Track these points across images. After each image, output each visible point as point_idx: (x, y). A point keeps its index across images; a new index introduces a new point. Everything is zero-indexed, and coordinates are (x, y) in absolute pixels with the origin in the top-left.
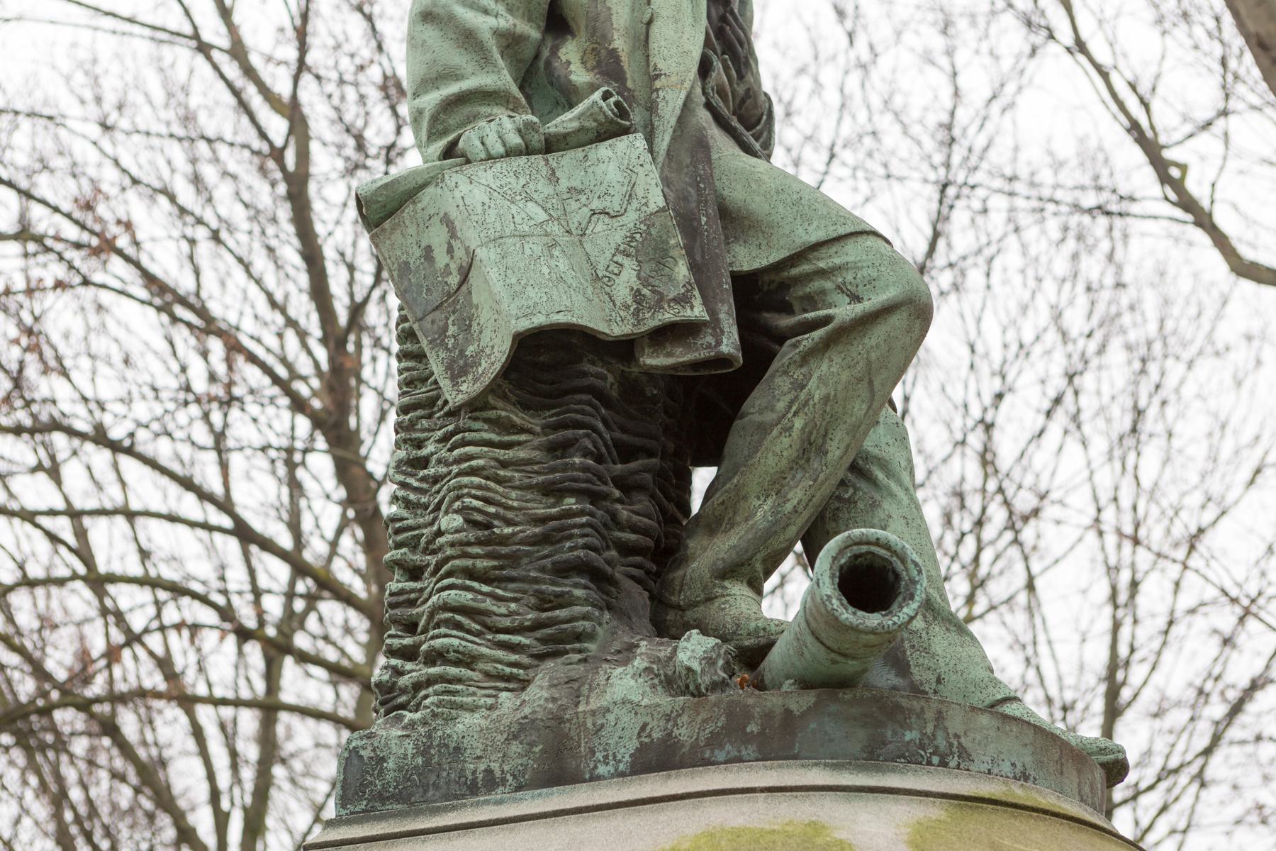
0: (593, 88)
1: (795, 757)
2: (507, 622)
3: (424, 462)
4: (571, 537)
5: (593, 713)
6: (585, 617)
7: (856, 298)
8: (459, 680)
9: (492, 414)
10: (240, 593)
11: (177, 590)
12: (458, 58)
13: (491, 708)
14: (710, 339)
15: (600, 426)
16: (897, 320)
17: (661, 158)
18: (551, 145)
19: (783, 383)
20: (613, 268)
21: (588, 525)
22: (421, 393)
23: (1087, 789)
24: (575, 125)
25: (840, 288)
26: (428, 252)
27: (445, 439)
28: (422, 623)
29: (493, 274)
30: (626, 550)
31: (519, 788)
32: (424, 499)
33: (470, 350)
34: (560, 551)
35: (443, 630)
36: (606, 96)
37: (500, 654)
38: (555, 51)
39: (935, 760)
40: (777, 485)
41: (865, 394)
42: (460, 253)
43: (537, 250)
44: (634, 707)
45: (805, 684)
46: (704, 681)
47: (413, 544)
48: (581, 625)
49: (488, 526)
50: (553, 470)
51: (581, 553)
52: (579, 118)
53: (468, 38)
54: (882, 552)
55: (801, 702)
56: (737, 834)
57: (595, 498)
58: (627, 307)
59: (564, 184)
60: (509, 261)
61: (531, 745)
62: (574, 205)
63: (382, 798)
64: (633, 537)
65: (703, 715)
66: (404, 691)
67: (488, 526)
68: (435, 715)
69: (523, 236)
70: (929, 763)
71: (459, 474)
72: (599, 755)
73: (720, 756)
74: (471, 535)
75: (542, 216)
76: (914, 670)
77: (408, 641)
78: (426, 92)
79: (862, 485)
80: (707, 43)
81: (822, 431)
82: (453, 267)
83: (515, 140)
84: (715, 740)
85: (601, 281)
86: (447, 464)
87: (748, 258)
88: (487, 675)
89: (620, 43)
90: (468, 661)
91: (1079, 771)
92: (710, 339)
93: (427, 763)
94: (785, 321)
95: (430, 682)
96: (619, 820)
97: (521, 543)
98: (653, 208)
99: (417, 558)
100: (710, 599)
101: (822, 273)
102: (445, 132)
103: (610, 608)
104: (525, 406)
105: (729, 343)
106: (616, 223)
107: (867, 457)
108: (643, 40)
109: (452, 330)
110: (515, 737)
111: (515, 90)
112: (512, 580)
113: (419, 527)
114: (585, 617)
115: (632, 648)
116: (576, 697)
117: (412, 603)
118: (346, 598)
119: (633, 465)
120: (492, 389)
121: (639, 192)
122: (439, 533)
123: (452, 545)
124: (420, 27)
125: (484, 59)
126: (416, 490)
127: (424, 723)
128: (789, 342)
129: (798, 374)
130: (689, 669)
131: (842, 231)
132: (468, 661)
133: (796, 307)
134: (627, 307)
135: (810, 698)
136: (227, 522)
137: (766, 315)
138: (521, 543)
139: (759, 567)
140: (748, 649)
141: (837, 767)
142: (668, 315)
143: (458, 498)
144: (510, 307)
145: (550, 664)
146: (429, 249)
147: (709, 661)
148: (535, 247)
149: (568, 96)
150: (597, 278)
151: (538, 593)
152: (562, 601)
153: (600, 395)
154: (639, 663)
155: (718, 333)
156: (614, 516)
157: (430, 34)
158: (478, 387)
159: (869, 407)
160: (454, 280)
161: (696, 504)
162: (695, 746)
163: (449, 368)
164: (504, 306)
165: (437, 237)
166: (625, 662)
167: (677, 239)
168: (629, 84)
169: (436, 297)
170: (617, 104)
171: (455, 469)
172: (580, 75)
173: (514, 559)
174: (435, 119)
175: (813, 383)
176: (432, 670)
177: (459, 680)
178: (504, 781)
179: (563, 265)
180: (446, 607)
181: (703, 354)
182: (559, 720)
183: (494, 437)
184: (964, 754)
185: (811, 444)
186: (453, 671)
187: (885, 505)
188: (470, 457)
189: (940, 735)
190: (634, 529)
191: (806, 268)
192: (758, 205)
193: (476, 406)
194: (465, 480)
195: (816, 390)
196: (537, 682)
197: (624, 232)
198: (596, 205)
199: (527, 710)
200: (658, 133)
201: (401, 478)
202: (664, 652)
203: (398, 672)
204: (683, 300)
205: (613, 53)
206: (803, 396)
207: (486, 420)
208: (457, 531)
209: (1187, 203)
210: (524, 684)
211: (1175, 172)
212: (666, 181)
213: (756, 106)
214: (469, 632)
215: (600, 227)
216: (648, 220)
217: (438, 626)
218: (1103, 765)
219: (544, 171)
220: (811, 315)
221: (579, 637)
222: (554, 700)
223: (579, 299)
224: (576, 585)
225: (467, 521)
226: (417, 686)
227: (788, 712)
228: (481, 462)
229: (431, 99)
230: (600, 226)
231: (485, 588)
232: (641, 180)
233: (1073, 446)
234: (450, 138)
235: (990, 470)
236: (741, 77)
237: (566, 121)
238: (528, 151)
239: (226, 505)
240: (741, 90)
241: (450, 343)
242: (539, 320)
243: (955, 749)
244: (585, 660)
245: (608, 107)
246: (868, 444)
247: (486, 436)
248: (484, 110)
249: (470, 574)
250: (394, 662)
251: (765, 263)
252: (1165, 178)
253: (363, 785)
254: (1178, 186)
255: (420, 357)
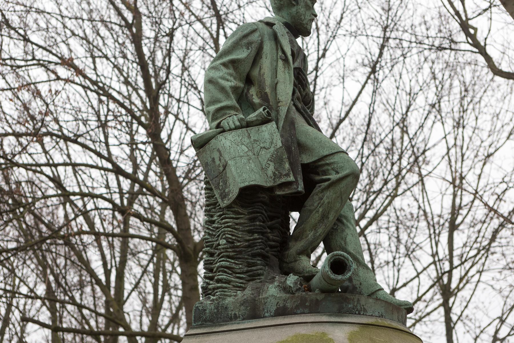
0: (261, 106)
1: (319, 313)
2: (239, 271)
3: (213, 222)
4: (256, 246)
5: (264, 298)
6: (261, 269)
7: (337, 173)
8: (226, 288)
9: (233, 209)
10: (115, 192)
11: (93, 196)
12: (220, 96)
13: (235, 296)
14: (295, 186)
15: (264, 212)
16: (349, 179)
17: (280, 129)
18: (249, 125)
19: (316, 198)
20: (267, 165)
21: (261, 242)
22: (212, 201)
23: (400, 317)
24: (255, 118)
25: (333, 169)
26: (213, 159)
27: (220, 216)
28: (215, 269)
29: (233, 169)
30: (271, 247)
31: (243, 319)
32: (214, 233)
33: (227, 190)
34: (253, 250)
35: (221, 273)
36: (264, 110)
37: (237, 280)
38: (248, 90)
39: (357, 312)
40: (315, 227)
42: (223, 161)
43: (245, 161)
44: (275, 297)
45: (323, 291)
46: (294, 289)
47: (211, 246)
48: (260, 271)
49: (233, 243)
50: (251, 226)
51: (259, 251)
52: (256, 116)
53: (222, 89)
54: (342, 258)
55: (321, 297)
56: (303, 336)
57: (262, 233)
58: (271, 177)
59: (252, 138)
60: (238, 165)
61: (247, 307)
62: (255, 145)
63: (205, 321)
64: (273, 243)
65: (294, 300)
66: (210, 289)
67: (233, 243)
68: (220, 298)
69: (241, 157)
70: (355, 314)
71: (225, 227)
72: (266, 311)
73: (299, 312)
74: (228, 246)
75: (247, 150)
76: (354, 281)
77: (210, 275)
78: (210, 106)
79: (340, 224)
80: (295, 85)
82: (221, 165)
83: (238, 123)
84: (297, 307)
85: (264, 169)
86: (221, 224)
87: (306, 159)
88: (234, 286)
89: (268, 90)
90: (228, 282)
91: (398, 312)
92: (295, 186)
93: (218, 311)
94: (318, 178)
95: (218, 288)
96: (271, 331)
97: (242, 247)
98: (278, 146)
99: (212, 251)
100: (296, 261)
101: (328, 164)
102: (216, 119)
103: (267, 265)
104: (242, 207)
105: (301, 188)
106: (268, 151)
107: (341, 216)
108: (275, 87)
109: (221, 184)
110: (242, 305)
111: (237, 105)
112: (240, 258)
113: (213, 241)
114: (261, 269)
115: (274, 278)
116: (259, 293)
117: (211, 264)
118: (153, 192)
119: (273, 222)
120: (234, 202)
121: (274, 142)
122: (219, 245)
123: (223, 249)
124: (208, 85)
125: (228, 96)
126: (211, 230)
127: (217, 300)
128: (318, 185)
129: (321, 195)
130: (290, 286)
131: (333, 151)
132: (228, 282)
133: (320, 173)
134: (271, 177)
135: (323, 296)
136: (109, 166)
137: (312, 175)
138: (242, 247)
139: (309, 251)
140: (307, 277)
141: (330, 315)
142: (283, 180)
143: (224, 234)
144: (238, 180)
145: (251, 283)
146: (214, 159)
147: (296, 283)
148: (244, 160)
149: (254, 107)
150: (262, 169)
151: (248, 263)
152: (254, 264)
153: (263, 203)
154: (276, 284)
155: (298, 185)
156: (268, 238)
157: (211, 87)
158: (229, 202)
160: (221, 169)
161: (292, 231)
162: (292, 309)
163: (221, 195)
164: (237, 179)
165: (216, 155)
166: (272, 282)
167: (285, 156)
168: (271, 103)
169: (216, 174)
170: (268, 112)
171: (223, 226)
172: (256, 100)
173: (240, 252)
174: (213, 115)
175: (325, 198)
176: (219, 285)
177: (226, 288)
178: (239, 317)
179: (253, 165)
180: (222, 267)
181: (293, 191)
182: (255, 300)
183: (234, 216)
184: (365, 310)
186: (224, 285)
187: (346, 230)
188: (227, 222)
189: (358, 305)
190: (274, 241)
191: (323, 162)
192: (309, 143)
193: (229, 207)
194: (226, 229)
195: (326, 200)
196: (248, 288)
197: (270, 154)
198: (262, 145)
199: (245, 297)
200: (280, 121)
201: (207, 226)
202: (283, 280)
203: (208, 284)
204: (287, 175)
205: (266, 93)
206: (322, 202)
207: (232, 211)
208: (224, 245)
209: (476, 44)
210: (244, 289)
211: (472, 31)
212: (282, 136)
213: (309, 97)
214: (228, 274)
215: (263, 152)
216: (277, 150)
217: (219, 272)
218: (405, 309)
219: (247, 134)
220: (324, 177)
221: (259, 275)
222: (253, 294)
223: (257, 176)
224: (258, 260)
225: (227, 241)
226: (214, 289)
227: (317, 300)
228: (230, 224)
229: (212, 108)
230: (263, 152)
231: (233, 261)
232: (275, 138)
233: (438, 124)
234: (218, 121)
236: (304, 90)
237: (252, 116)
238: (241, 127)
239: (109, 159)
240: (304, 94)
241: (221, 188)
242: (247, 184)
244: (261, 282)
245: (265, 113)
246: (342, 212)
247: (232, 216)
248: (228, 112)
249: (229, 257)
250: (207, 281)
251: (311, 161)
252: (468, 34)
253: (200, 317)
254: (473, 37)
255: (211, 189)
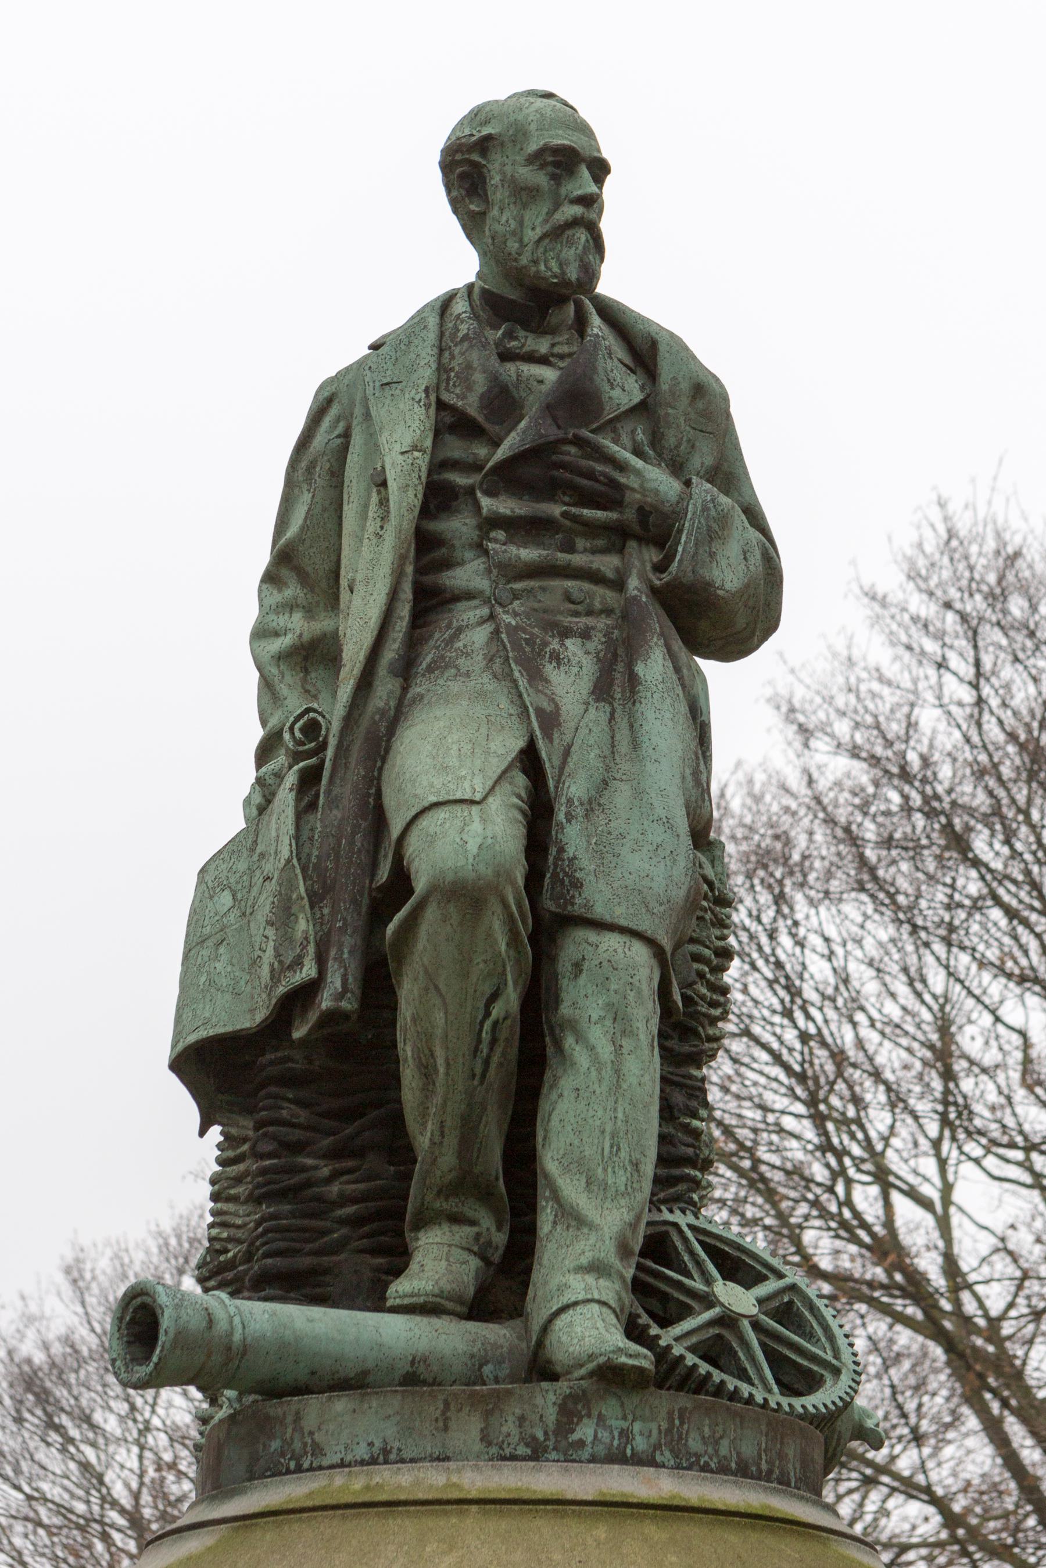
41: (438, 1001)
81: (427, 1052)
159: (446, 1013)
185: (426, 1067)
190: (354, 1200)
235: (772, 959)
243: (309, 1449)
